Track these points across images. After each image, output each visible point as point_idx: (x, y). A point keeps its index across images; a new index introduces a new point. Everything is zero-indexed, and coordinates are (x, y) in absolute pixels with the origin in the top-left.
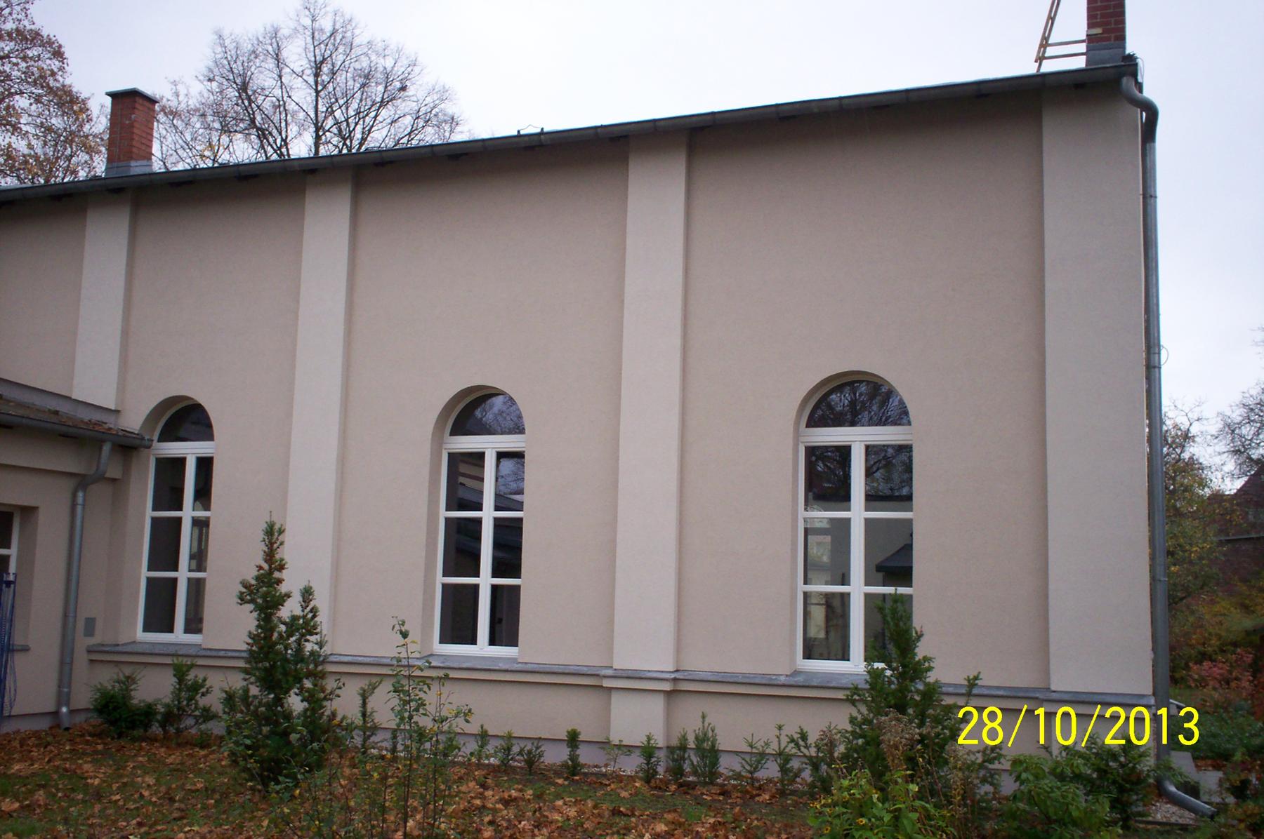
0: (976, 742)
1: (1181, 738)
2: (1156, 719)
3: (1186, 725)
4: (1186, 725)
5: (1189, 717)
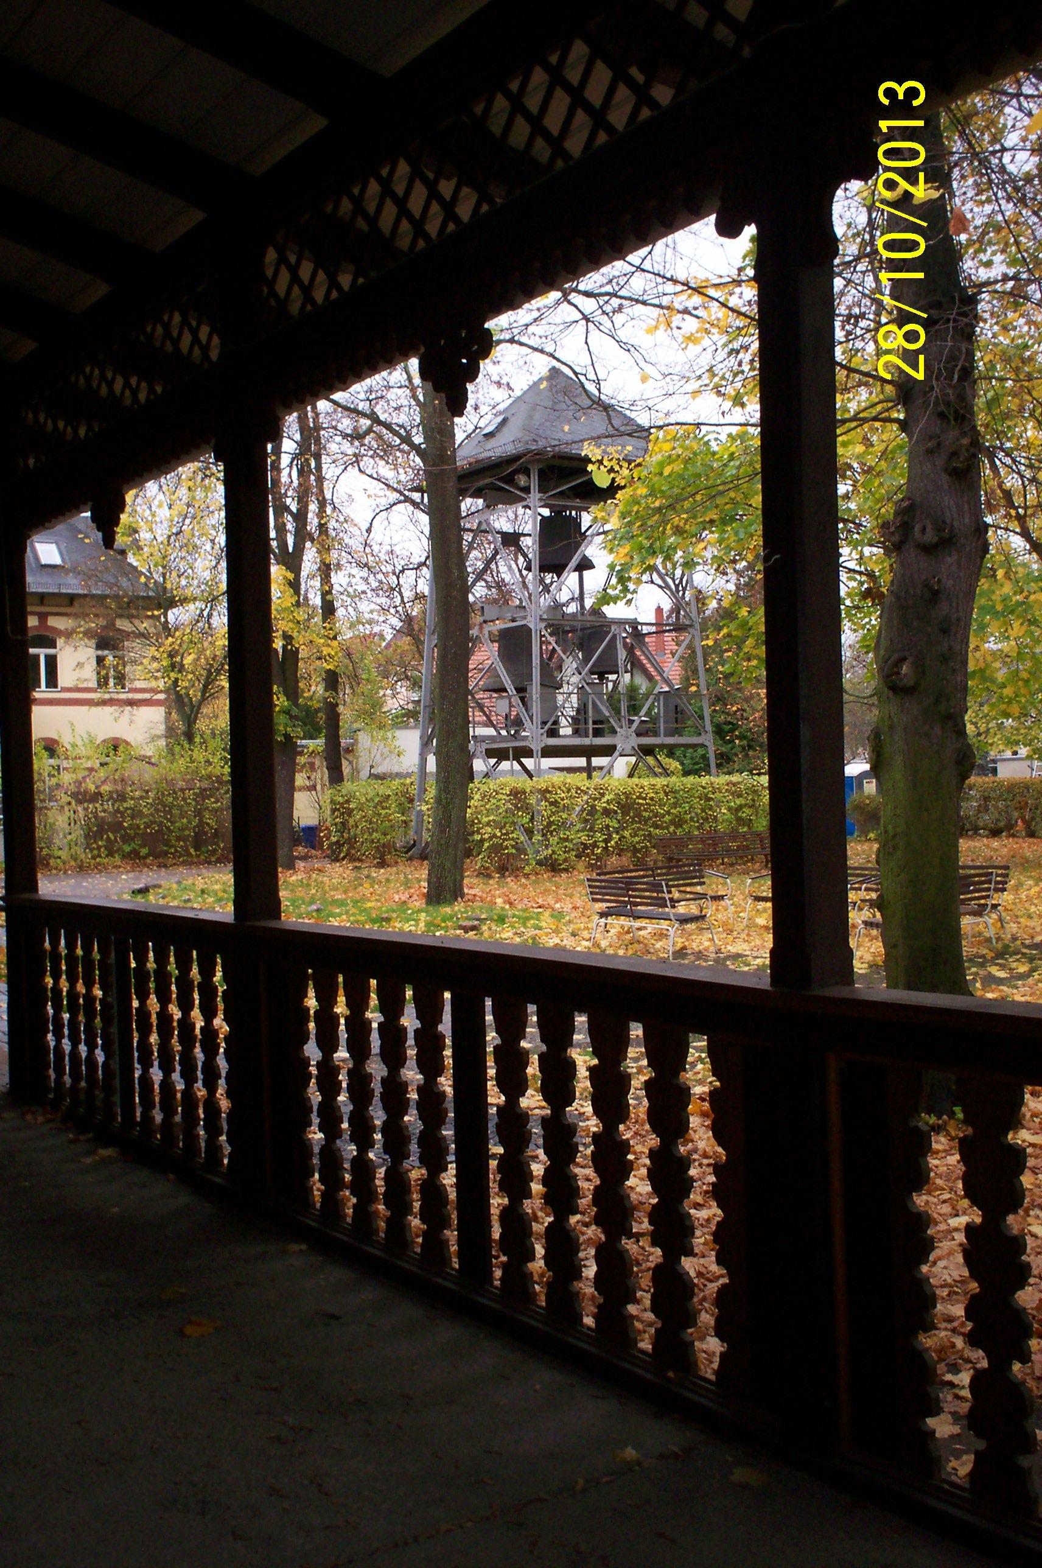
0: (921, 358)
1: (916, 103)
2: (894, 134)
3: (901, 97)
4: (901, 97)
5: (891, 93)
